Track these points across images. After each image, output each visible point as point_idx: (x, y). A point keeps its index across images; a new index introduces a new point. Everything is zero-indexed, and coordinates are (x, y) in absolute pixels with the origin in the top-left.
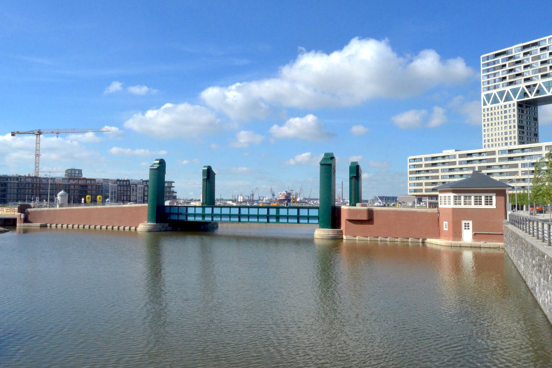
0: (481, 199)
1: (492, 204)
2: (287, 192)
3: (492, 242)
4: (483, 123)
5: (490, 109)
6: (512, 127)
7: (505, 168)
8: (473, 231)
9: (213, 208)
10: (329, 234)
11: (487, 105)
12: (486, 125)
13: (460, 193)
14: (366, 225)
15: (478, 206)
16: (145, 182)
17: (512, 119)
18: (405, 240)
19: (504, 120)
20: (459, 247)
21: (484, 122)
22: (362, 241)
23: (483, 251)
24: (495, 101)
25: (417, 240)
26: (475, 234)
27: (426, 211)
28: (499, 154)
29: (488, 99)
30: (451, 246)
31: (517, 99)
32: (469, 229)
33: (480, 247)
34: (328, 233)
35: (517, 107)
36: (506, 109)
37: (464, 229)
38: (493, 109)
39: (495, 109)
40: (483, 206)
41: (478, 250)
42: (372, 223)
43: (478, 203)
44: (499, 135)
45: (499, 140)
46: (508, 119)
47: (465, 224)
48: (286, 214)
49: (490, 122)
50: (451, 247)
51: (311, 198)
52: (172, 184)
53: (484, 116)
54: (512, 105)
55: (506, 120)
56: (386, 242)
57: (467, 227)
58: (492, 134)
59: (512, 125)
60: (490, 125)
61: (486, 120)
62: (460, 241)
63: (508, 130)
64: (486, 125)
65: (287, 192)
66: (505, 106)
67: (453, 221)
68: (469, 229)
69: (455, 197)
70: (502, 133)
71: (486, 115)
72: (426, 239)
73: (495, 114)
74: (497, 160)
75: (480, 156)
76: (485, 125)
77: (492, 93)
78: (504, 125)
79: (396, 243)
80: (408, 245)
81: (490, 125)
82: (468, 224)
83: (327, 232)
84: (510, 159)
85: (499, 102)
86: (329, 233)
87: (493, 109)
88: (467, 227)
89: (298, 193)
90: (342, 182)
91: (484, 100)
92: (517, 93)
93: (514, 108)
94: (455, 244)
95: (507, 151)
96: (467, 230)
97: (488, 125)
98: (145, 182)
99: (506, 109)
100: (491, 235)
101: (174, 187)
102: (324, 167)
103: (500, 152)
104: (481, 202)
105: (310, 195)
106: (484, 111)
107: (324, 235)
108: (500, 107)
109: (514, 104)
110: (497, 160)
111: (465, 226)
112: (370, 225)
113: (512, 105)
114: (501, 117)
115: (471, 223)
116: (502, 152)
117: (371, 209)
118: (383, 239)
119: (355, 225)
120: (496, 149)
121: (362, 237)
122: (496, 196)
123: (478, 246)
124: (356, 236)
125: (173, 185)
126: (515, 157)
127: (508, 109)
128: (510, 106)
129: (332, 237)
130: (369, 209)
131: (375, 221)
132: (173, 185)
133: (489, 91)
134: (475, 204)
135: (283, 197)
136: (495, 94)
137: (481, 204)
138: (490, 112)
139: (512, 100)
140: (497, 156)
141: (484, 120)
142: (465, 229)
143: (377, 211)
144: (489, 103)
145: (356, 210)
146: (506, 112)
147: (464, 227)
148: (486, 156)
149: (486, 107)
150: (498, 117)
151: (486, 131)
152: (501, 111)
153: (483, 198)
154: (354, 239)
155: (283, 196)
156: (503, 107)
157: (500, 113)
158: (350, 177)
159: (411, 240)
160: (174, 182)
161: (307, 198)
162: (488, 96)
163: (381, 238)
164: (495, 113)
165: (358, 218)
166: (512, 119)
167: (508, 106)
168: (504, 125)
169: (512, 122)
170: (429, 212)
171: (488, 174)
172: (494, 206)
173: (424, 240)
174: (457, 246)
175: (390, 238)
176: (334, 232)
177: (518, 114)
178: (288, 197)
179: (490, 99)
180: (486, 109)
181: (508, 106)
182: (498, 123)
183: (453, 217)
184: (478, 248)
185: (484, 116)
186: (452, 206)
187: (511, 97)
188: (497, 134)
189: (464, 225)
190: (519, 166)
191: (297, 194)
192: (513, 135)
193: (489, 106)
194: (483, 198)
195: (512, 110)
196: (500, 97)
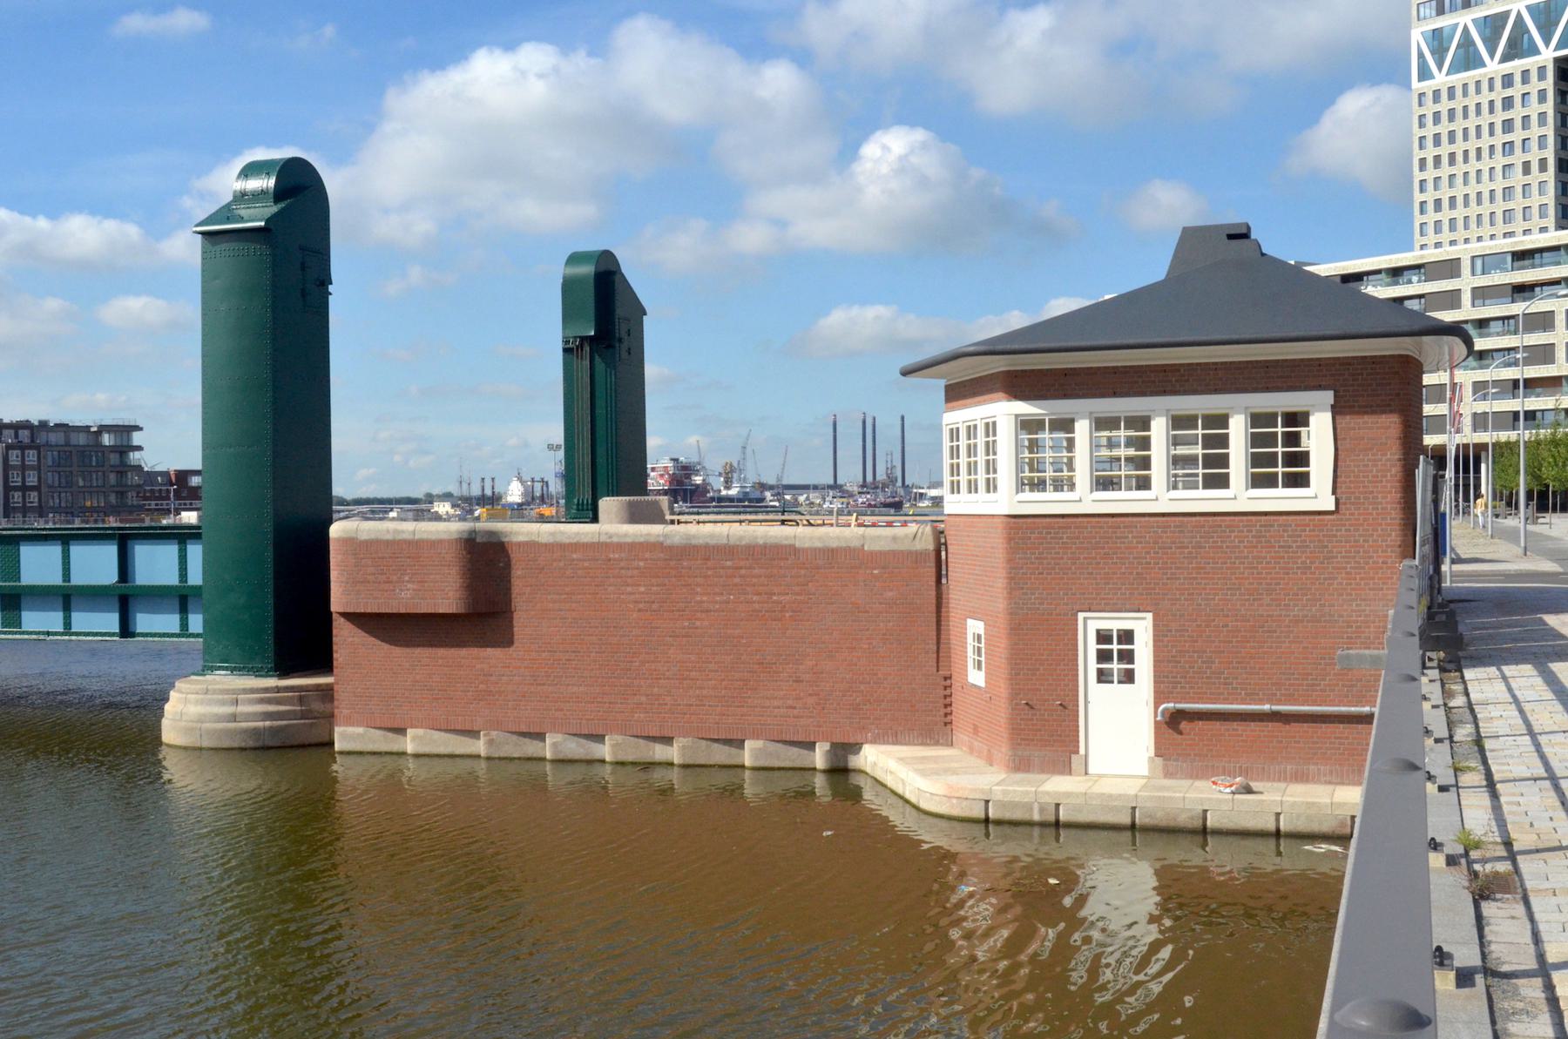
0: (1223, 441)
1: (1300, 481)
2: (675, 460)
3: (1300, 777)
4: (1418, 154)
5: (1444, 95)
6: (1535, 167)
7: (1498, 334)
8: (1159, 697)
9: (124, 542)
10: (234, 718)
11: (1432, 77)
12: (1430, 162)
13: (1066, 396)
14: (464, 652)
15: (1280, 491)
16: (12, 432)
17: (1535, 131)
18: (721, 754)
19: (1500, 138)
20: (1043, 825)
21: (1421, 147)
22: (439, 766)
23: (1224, 861)
24: (1469, 59)
25: (795, 750)
26: (1172, 722)
27: (855, 544)
28: (1473, 274)
29: (1439, 52)
30: (987, 820)
31: (1555, 50)
32: (1129, 677)
33: (1202, 833)
34: (229, 709)
35: (1555, 84)
36: (1508, 92)
37: (1093, 675)
38: (1459, 92)
39: (1465, 94)
40: (1240, 496)
41: (1188, 855)
42: (504, 638)
43: (1280, 470)
44: (1479, 202)
45: (1479, 222)
46: (1517, 136)
47: (1103, 637)
48: (56, 579)
49: (1445, 150)
50: (981, 828)
51: (785, 482)
52: (129, 438)
53: (1422, 125)
54: (1534, 75)
55: (1508, 138)
56: (597, 768)
57: (1115, 666)
58: (1452, 199)
59: (1534, 156)
60: (1445, 160)
61: (1429, 142)
62: (1065, 768)
63: (1517, 179)
64: (1430, 162)
65: (675, 460)
66: (1508, 80)
67: (1012, 614)
68: (1129, 677)
69: (1028, 425)
70: (1492, 191)
71: (1429, 120)
72: (855, 748)
73: (1466, 116)
74: (1466, 298)
75: (1397, 283)
76: (1423, 162)
77: (1457, 25)
78: (1500, 161)
79: (658, 775)
80: (735, 790)
81: (1445, 160)
82: (1127, 636)
83: (223, 703)
84: (1522, 290)
85: (1483, 65)
86: (242, 709)
87: (1459, 92)
88: (1115, 666)
89: (735, 465)
90: (903, 418)
91: (1421, 55)
92: (1557, 24)
93: (1542, 85)
94: (1014, 805)
95: (1509, 258)
96: (1115, 689)
97: (1437, 159)
98: (12, 432)
99: (1508, 92)
100: (1295, 727)
101: (139, 448)
102: (225, 247)
103: (1479, 263)
104: (1223, 461)
105: (782, 472)
106: (1420, 105)
107: (201, 719)
108: (1485, 86)
109: (1542, 70)
110: (1466, 298)
111: (1104, 656)
112: (489, 651)
113: (1534, 75)
114: (1492, 125)
115: (1143, 627)
116: (1487, 262)
117: (492, 533)
118: (575, 748)
119: (398, 651)
120: (1463, 252)
121: (437, 735)
122: (1337, 410)
123: (1183, 820)
124: (401, 731)
125: (137, 439)
126: (1541, 250)
127: (1516, 91)
128: (1525, 74)
129: (256, 732)
130: (473, 532)
131: (523, 620)
132: (137, 439)
133: (1441, 17)
134: (1259, 481)
135: (662, 482)
136: (1466, 27)
137: (1144, 484)
138: (1444, 106)
139: (1536, 52)
140: (1466, 283)
141: (1422, 138)
142: (1103, 677)
143: (532, 546)
144: (1440, 68)
145: (389, 543)
146: (1508, 103)
147: (1093, 666)
148: (1419, 281)
149: (1428, 86)
150: (1478, 128)
151: (1430, 185)
152: (1491, 103)
153: (1238, 430)
154: (395, 748)
155: (662, 476)
156: (1498, 84)
157: (1485, 108)
158: (566, 342)
159: (756, 753)
160: (138, 428)
161: (772, 481)
162: (1438, 41)
163: (559, 738)
164: (1465, 108)
165: (406, 598)
166: (1535, 131)
167: (1518, 78)
168: (1500, 161)
169: (1534, 144)
170: (876, 547)
171: (1348, 279)
172: (1318, 494)
173: (844, 750)
174: (1030, 824)
175: (619, 738)
176: (278, 702)
177: (1557, 111)
178: (680, 483)
179: (1447, 49)
180: (1430, 95)
181: (1518, 78)
182: (1479, 150)
183: (1015, 583)
184: (1185, 842)
185: (1422, 125)
186: (1007, 500)
187: (1531, 39)
188: (1473, 197)
189: (1093, 647)
190: (1557, 323)
191: (732, 470)
192: (1535, 201)
193: (1441, 79)
194: (1238, 430)
195: (1534, 98)
196: (1485, 41)
